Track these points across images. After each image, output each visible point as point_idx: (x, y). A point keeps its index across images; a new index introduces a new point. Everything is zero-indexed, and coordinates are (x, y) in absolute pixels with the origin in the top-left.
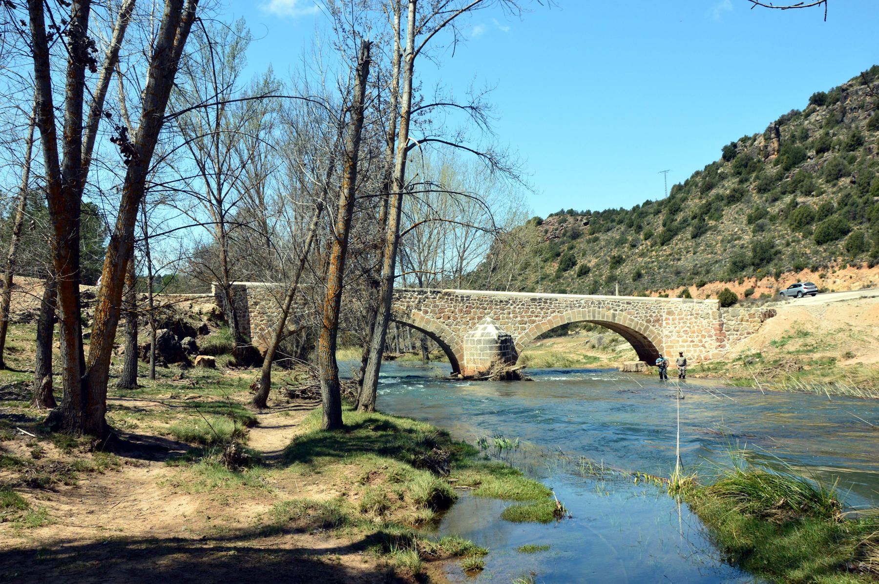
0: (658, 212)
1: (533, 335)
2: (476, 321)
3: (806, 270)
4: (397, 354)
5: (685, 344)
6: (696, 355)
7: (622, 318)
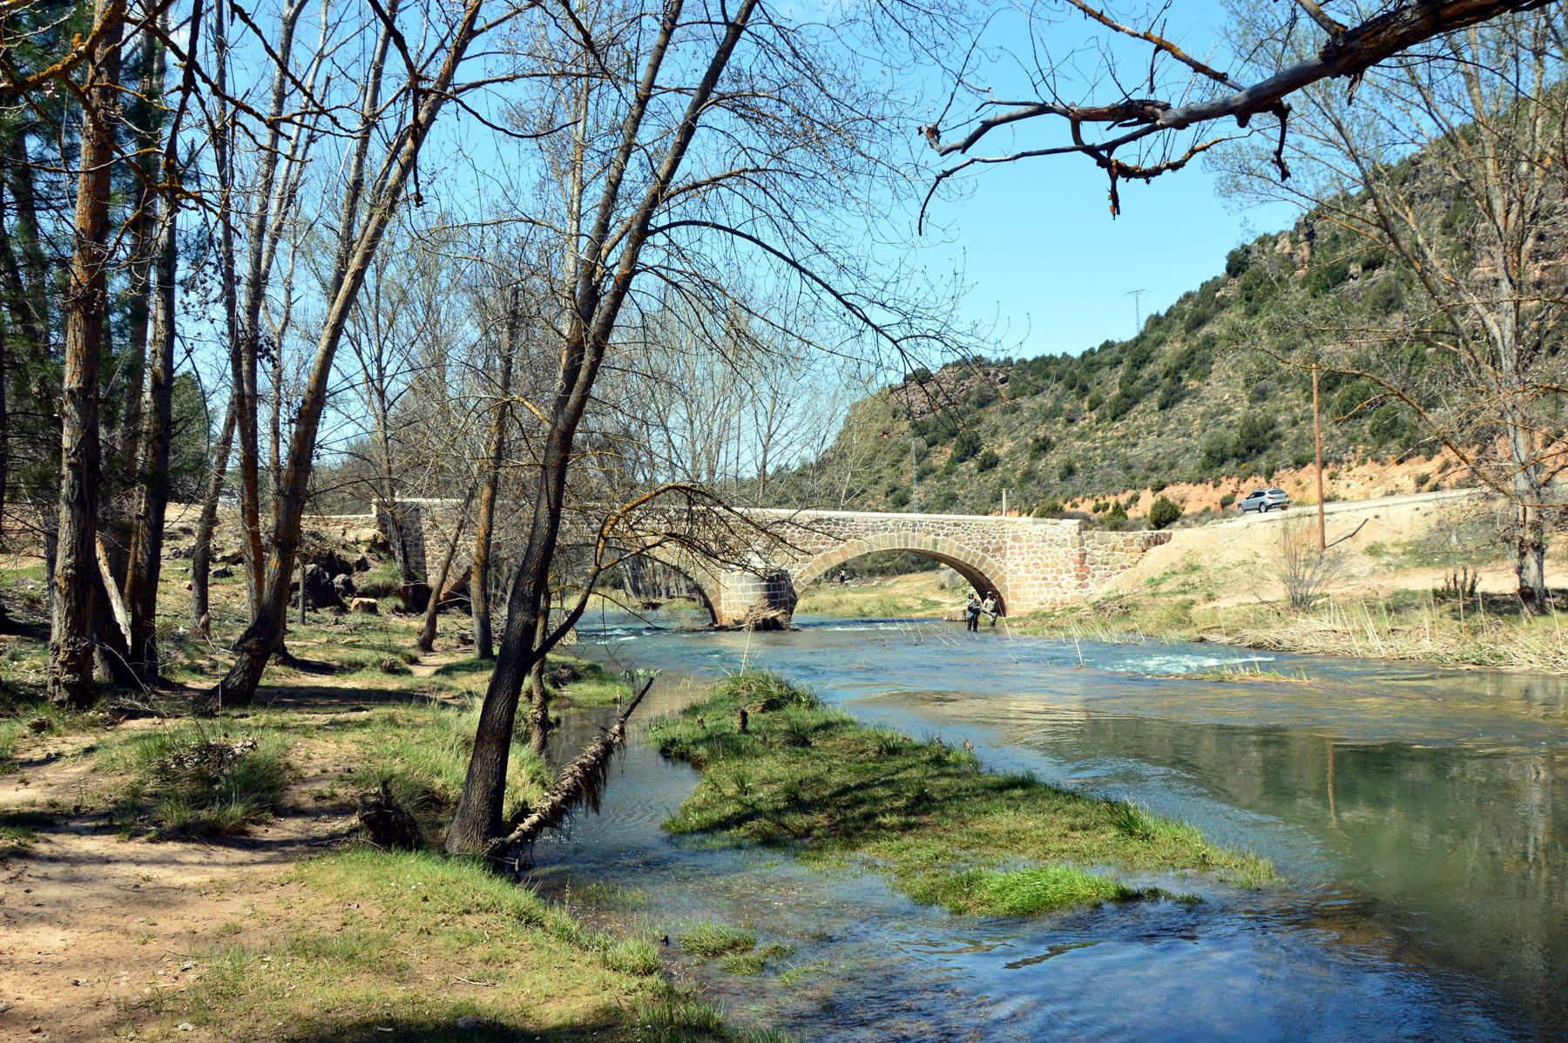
0: (1116, 363)
3: (1310, 466)
4: (664, 599)
5: (1036, 583)
6: (1049, 598)
7: (947, 546)
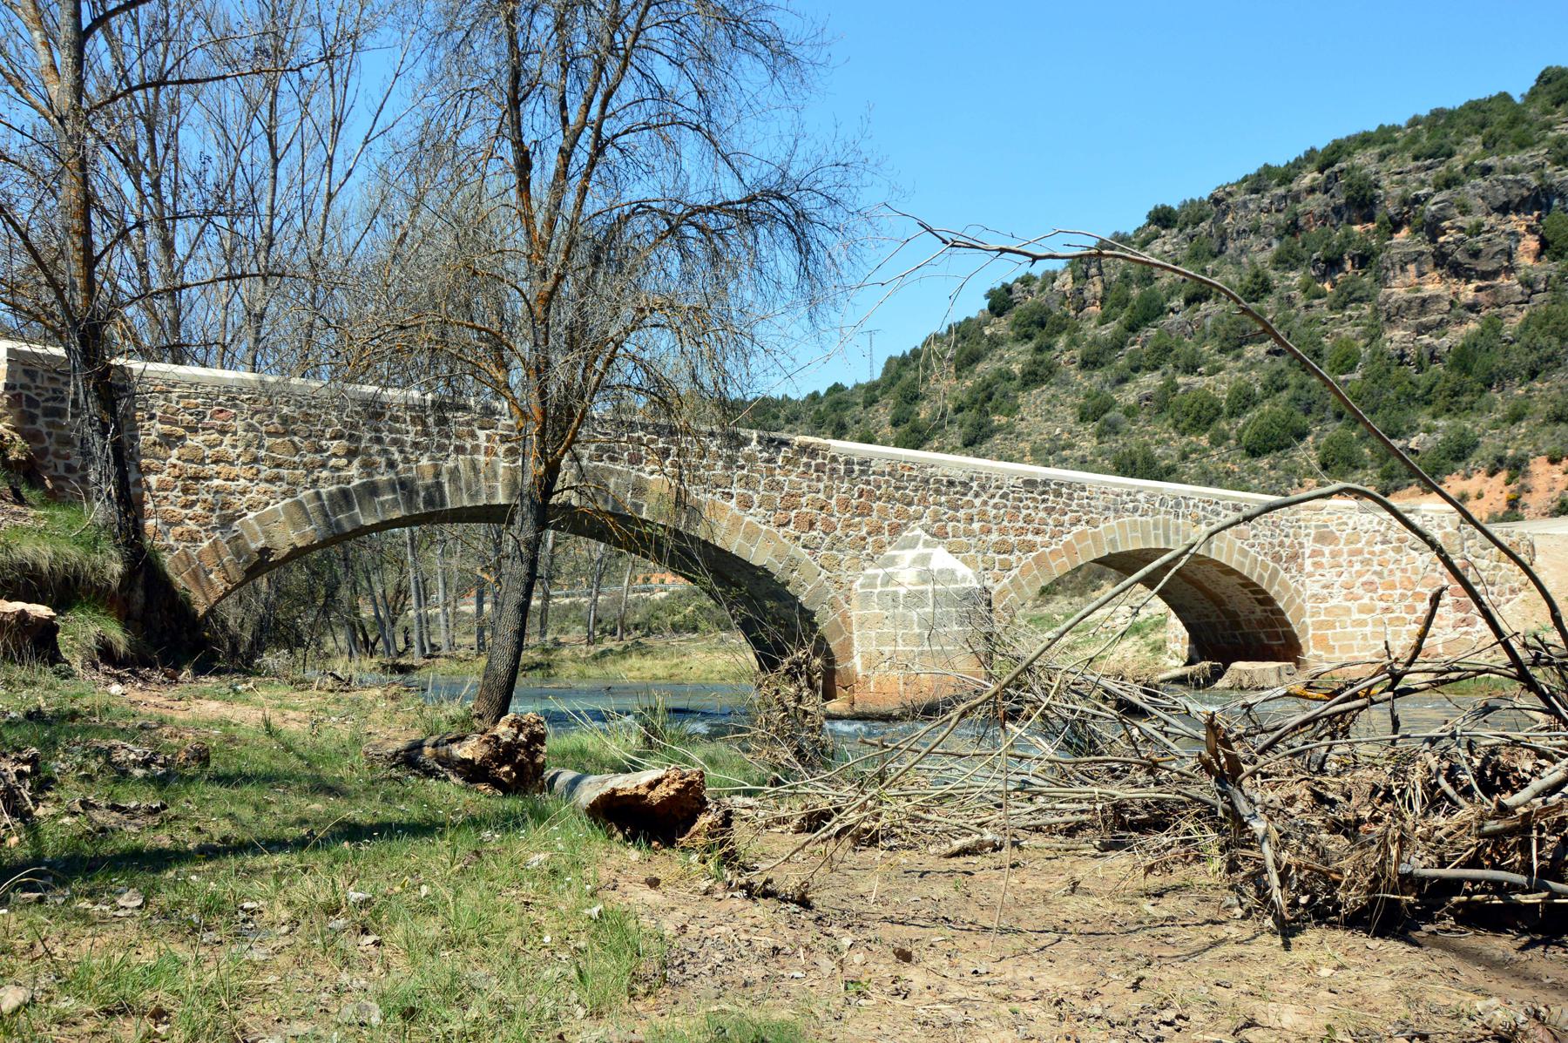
1: (1029, 584)
2: (886, 537)
